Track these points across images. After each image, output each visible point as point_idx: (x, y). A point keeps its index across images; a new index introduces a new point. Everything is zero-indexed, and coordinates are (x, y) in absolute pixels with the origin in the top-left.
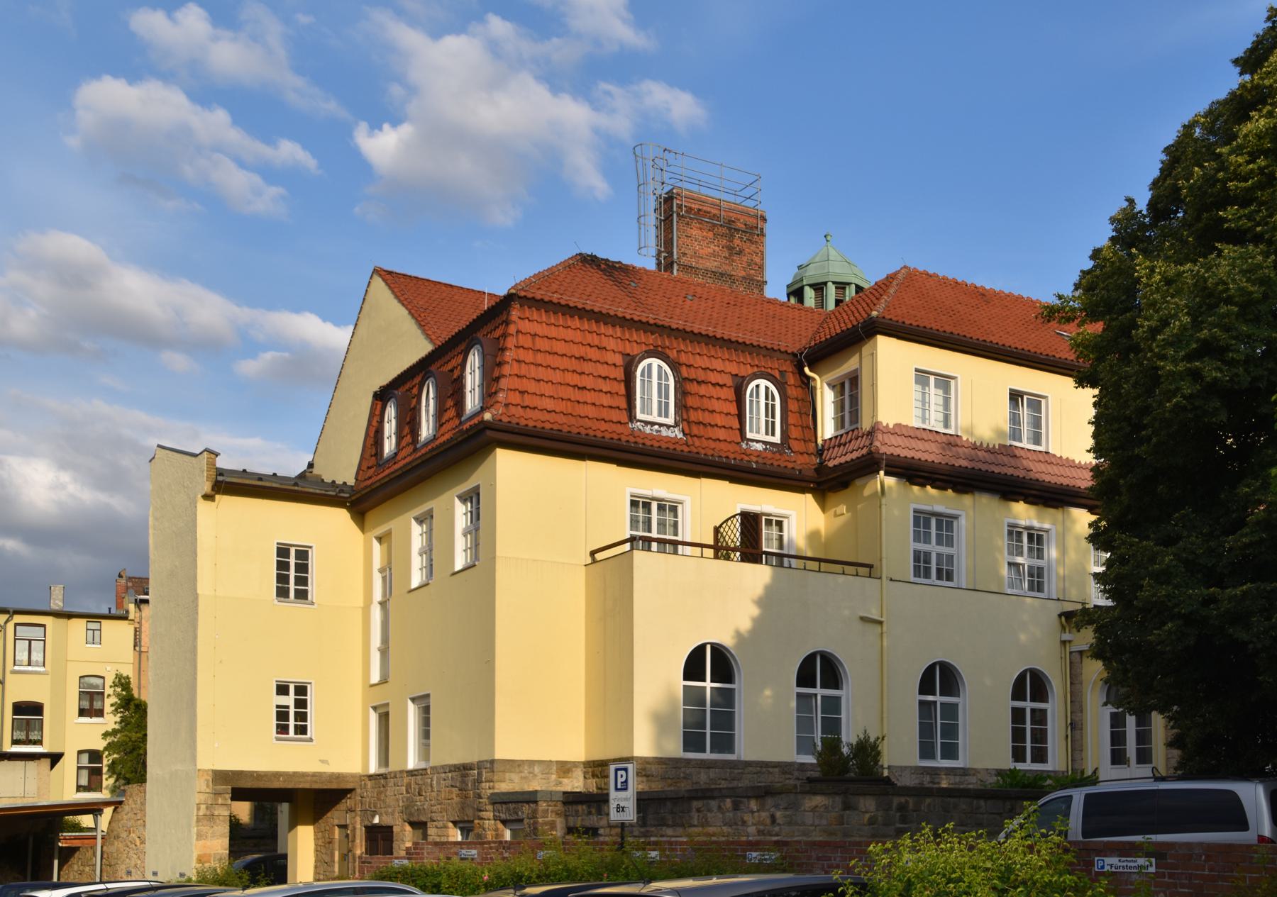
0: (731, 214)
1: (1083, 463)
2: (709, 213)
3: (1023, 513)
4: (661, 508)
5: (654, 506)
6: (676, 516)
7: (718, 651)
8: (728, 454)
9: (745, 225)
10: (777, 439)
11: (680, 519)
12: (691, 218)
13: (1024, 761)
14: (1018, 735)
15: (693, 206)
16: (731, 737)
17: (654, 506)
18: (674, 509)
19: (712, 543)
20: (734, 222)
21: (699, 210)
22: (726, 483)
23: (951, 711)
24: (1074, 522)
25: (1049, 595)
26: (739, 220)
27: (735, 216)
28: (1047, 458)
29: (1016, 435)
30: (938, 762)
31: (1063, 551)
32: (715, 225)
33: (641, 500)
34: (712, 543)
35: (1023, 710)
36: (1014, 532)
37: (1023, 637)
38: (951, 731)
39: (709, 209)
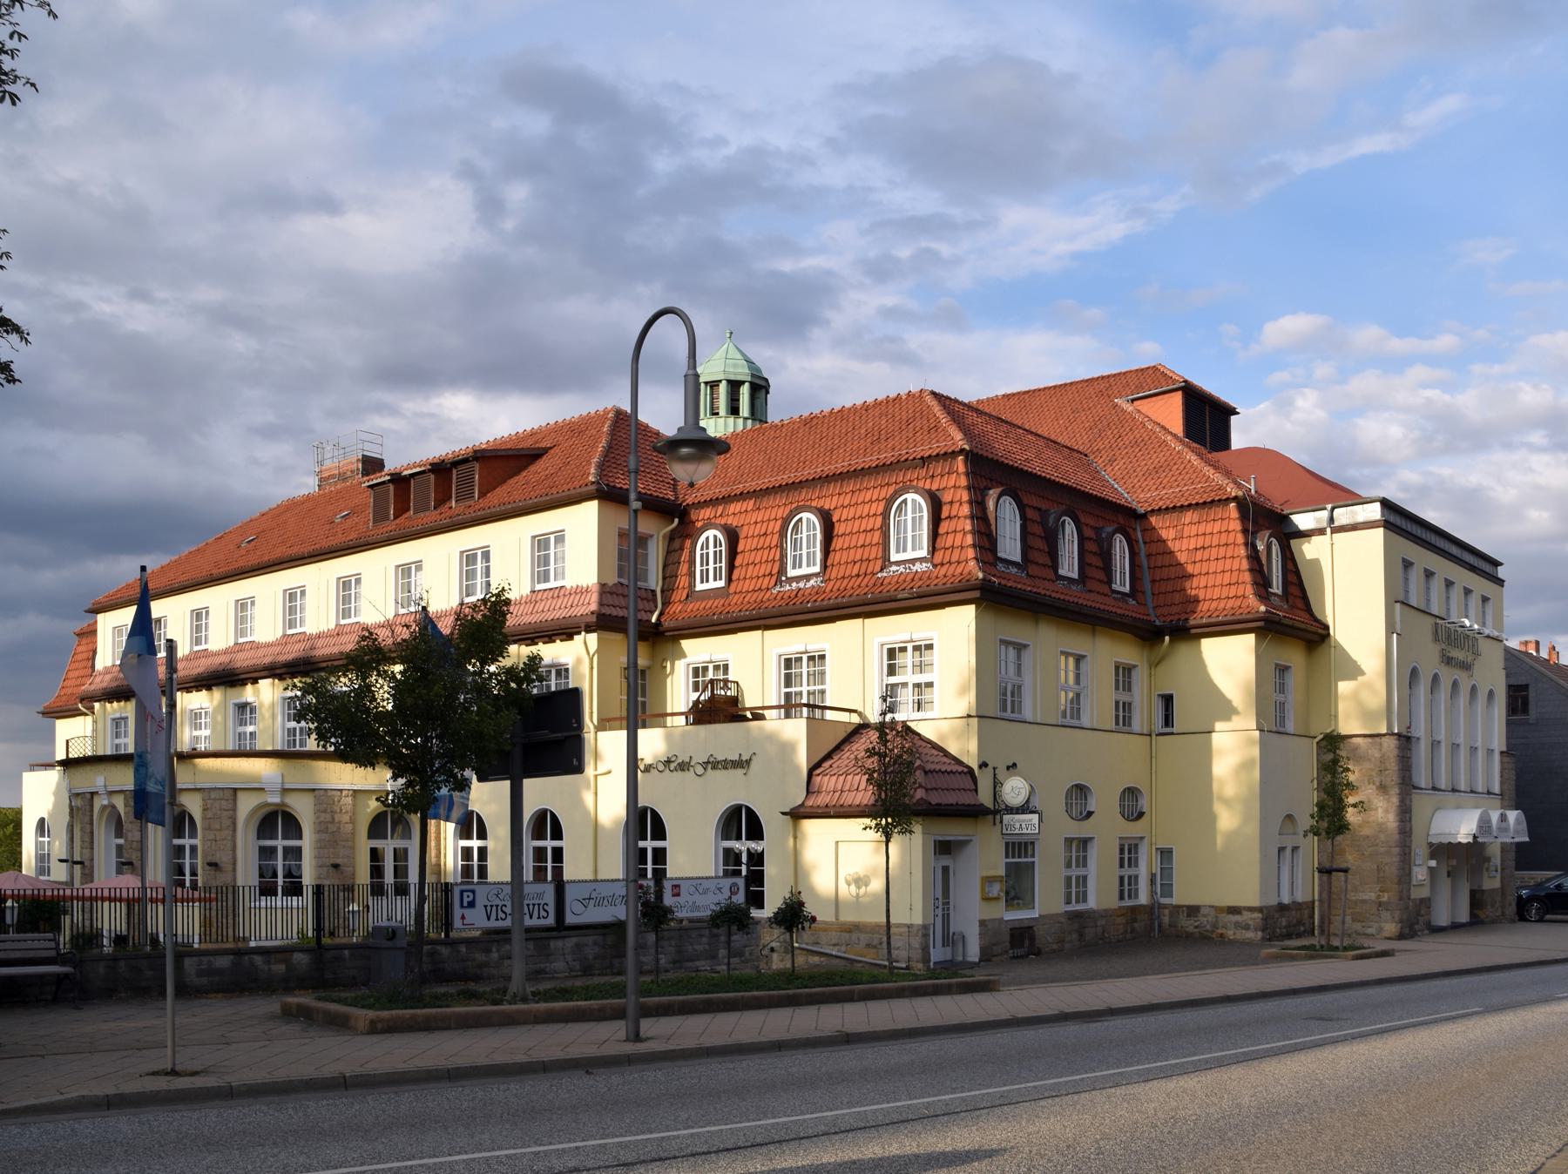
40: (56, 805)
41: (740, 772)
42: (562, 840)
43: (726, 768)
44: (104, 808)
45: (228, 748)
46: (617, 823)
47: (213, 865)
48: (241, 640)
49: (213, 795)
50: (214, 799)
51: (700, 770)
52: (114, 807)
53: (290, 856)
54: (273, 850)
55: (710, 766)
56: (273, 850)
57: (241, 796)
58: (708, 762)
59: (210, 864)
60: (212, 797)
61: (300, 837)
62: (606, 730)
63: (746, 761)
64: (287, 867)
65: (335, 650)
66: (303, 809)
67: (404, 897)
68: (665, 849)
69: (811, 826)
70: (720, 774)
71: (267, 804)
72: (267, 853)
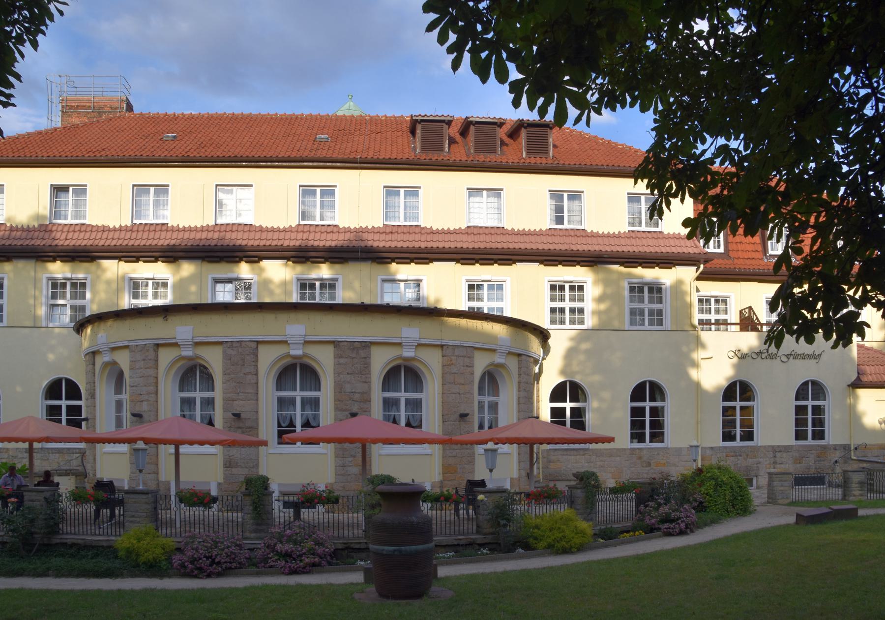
0: (101, 104)
1: (181, 227)
2: (85, 106)
3: (58, 269)
4: (717, 301)
5: (713, 300)
6: (726, 305)
7: (815, 383)
8: (740, 266)
9: (111, 108)
10: (721, 250)
11: (728, 307)
12: (71, 112)
13: (644, 441)
14: (800, 423)
15: (74, 104)
16: (823, 432)
17: (713, 300)
18: (725, 302)
19: (739, 322)
20: (103, 108)
21: (78, 106)
22: (756, 283)
23: (817, 410)
24: (104, 270)
25: (34, 324)
26: (106, 106)
27: (104, 104)
28: (660, 236)
29: (57, 215)
30: (810, 442)
31: (94, 293)
32: (88, 113)
33: (705, 298)
34: (739, 322)
35: (59, 407)
36: (57, 286)
37: (51, 357)
38: (819, 423)
39: (84, 104)
40: (594, 235)
41: (813, 361)
42: (796, 406)
43: (772, 358)
44: (106, 365)
45: (225, 299)
46: (718, 389)
47: (137, 416)
48: (137, 222)
49: (457, 352)
50: (458, 356)
51: (784, 359)
52: (114, 363)
53: (308, 407)
54: (292, 401)
55: (792, 357)
56: (292, 401)
57: (262, 349)
58: (791, 354)
59: (134, 415)
60: (457, 354)
61: (318, 388)
62: (748, 331)
63: (819, 355)
64: (304, 417)
65: (321, 244)
66: (214, 359)
67: (837, 489)
68: (723, 401)
69: (862, 393)
70: (799, 362)
71: (288, 355)
72: (284, 403)
